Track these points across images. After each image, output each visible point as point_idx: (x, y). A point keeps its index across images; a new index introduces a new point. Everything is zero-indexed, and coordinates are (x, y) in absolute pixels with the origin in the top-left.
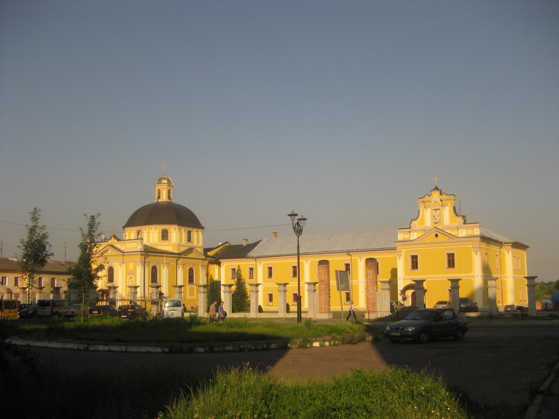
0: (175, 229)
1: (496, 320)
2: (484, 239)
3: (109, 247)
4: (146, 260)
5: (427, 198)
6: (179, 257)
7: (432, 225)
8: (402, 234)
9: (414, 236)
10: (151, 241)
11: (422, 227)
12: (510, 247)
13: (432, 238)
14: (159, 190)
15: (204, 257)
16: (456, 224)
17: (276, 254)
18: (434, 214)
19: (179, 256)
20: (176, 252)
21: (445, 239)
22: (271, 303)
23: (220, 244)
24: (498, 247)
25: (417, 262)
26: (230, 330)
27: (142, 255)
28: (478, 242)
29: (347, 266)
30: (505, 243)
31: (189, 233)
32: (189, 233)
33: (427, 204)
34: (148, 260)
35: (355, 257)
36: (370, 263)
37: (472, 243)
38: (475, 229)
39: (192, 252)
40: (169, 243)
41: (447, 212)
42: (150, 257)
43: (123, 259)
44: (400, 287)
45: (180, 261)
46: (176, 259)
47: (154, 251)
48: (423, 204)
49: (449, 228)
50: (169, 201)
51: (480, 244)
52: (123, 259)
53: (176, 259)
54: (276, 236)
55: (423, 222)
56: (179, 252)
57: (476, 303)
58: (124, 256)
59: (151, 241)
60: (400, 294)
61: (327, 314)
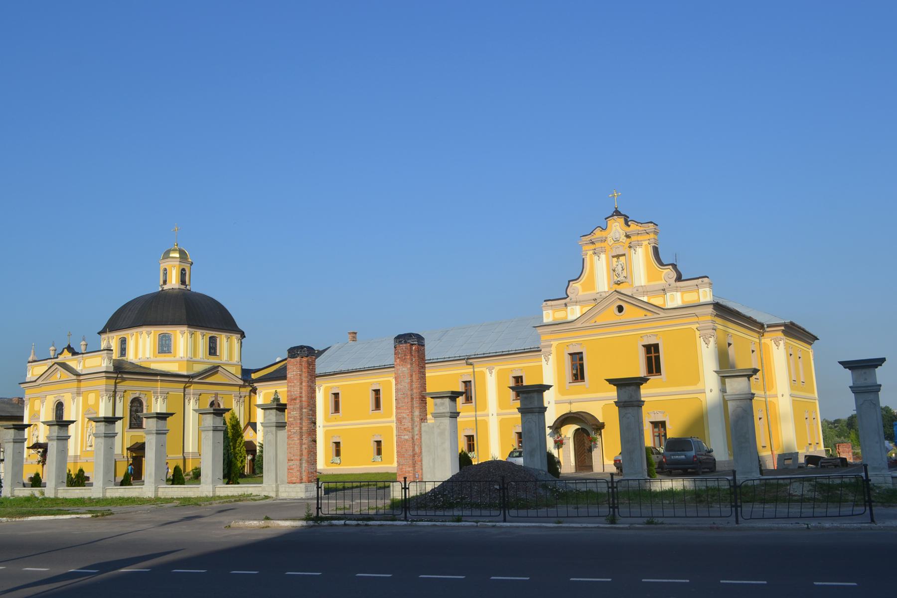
0: (183, 333)
2: (722, 311)
4: (119, 387)
5: (598, 234)
6: (188, 382)
7: (610, 288)
8: (550, 312)
9: (574, 312)
10: (140, 356)
11: (590, 294)
12: (780, 335)
13: (610, 313)
14: (165, 270)
15: (241, 383)
17: (344, 369)
18: (615, 264)
19: (189, 379)
20: (185, 373)
21: (640, 314)
22: (337, 460)
23: (278, 360)
24: (756, 335)
25: (582, 366)
26: (103, 528)
27: (108, 378)
28: (709, 318)
29: (467, 383)
30: (769, 326)
31: (213, 341)
32: (213, 341)
33: (598, 245)
34: (122, 386)
35: (481, 368)
36: (404, 346)
37: (695, 319)
39: (217, 372)
43: (78, 388)
44: (550, 418)
45: (192, 389)
47: (143, 371)
49: (645, 293)
50: (183, 287)
51: (713, 322)
52: (78, 388)
54: (354, 339)
58: (80, 381)
59: (140, 356)
61: (303, 486)
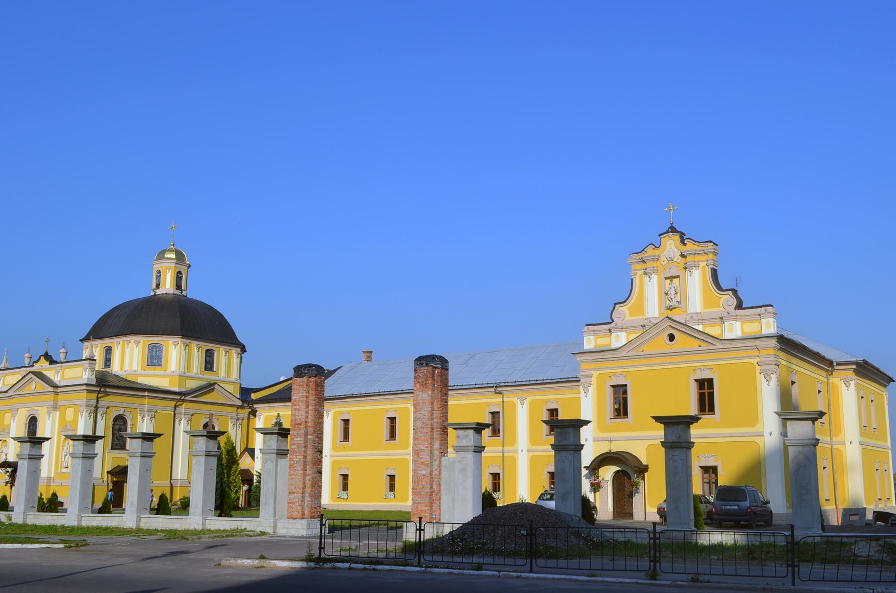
0: (176, 344)
1: (818, 568)
2: (787, 344)
3: (31, 375)
7: (661, 314)
8: (592, 337)
9: (619, 339)
11: (638, 319)
12: (851, 374)
13: (661, 343)
14: (159, 272)
15: (240, 403)
16: (719, 310)
19: (181, 396)
20: (176, 389)
21: (694, 344)
23: (282, 379)
24: (824, 373)
26: (77, 560)
27: (89, 391)
28: (772, 352)
30: (839, 364)
31: (209, 354)
32: (209, 354)
33: (649, 264)
37: (756, 353)
38: (763, 321)
39: (212, 390)
40: (163, 372)
41: (696, 282)
42: (110, 398)
43: (55, 401)
44: (587, 457)
45: (183, 408)
46: (174, 403)
47: (128, 385)
48: (643, 266)
49: (700, 321)
50: (178, 292)
51: (776, 356)
52: (55, 401)
53: (174, 403)
54: (369, 359)
55: (640, 308)
56: (183, 390)
57: (767, 502)
58: (57, 393)
59: (127, 368)
60: (587, 476)
61: (304, 522)
